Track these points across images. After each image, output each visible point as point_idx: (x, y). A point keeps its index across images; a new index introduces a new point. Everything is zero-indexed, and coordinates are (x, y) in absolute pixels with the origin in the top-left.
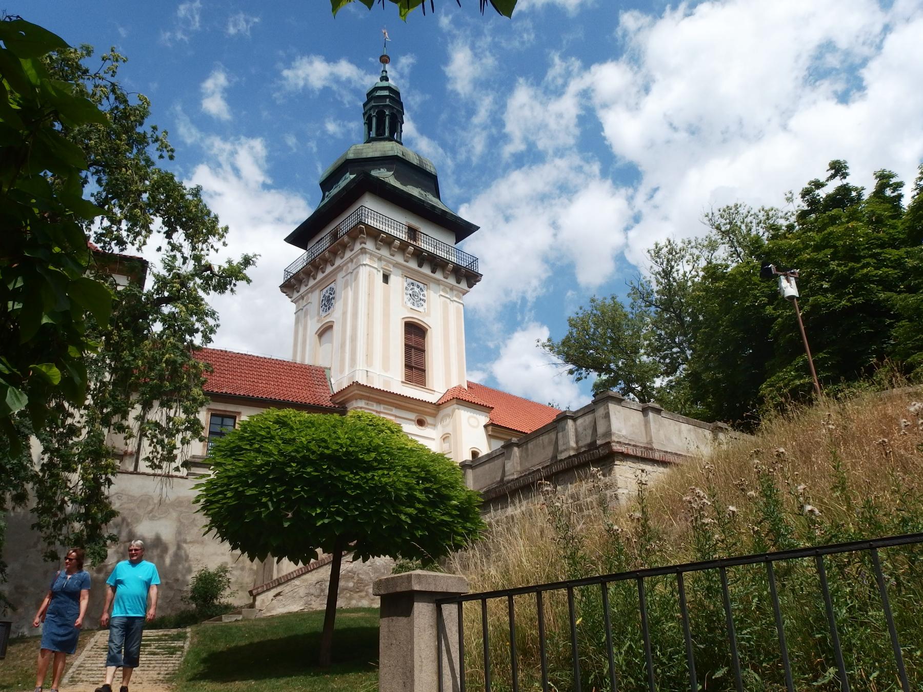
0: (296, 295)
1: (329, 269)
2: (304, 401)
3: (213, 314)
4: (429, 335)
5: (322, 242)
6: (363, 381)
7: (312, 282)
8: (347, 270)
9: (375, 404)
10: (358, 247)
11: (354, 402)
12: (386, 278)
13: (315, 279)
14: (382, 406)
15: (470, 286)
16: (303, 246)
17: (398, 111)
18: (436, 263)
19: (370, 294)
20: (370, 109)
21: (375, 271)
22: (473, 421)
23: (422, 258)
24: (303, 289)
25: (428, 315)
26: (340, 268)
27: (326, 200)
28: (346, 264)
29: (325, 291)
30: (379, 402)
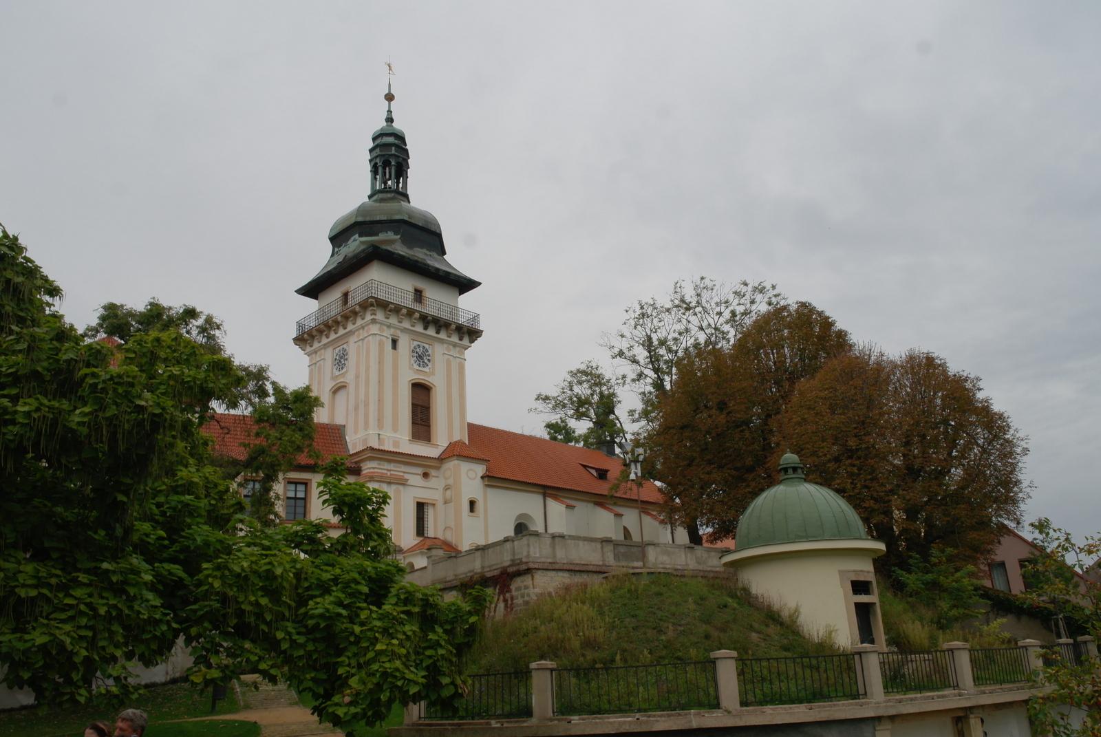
0: (309, 349)
1: (341, 332)
3: (191, 313)
5: (333, 296)
6: (376, 446)
7: (325, 341)
9: (386, 463)
10: (369, 317)
11: (368, 462)
14: (392, 465)
15: (472, 341)
18: (440, 324)
19: (381, 362)
20: (376, 157)
21: (384, 339)
22: (472, 474)
23: (426, 321)
24: (316, 345)
25: (433, 374)
26: (351, 333)
27: (339, 258)
29: (337, 350)
30: (389, 461)
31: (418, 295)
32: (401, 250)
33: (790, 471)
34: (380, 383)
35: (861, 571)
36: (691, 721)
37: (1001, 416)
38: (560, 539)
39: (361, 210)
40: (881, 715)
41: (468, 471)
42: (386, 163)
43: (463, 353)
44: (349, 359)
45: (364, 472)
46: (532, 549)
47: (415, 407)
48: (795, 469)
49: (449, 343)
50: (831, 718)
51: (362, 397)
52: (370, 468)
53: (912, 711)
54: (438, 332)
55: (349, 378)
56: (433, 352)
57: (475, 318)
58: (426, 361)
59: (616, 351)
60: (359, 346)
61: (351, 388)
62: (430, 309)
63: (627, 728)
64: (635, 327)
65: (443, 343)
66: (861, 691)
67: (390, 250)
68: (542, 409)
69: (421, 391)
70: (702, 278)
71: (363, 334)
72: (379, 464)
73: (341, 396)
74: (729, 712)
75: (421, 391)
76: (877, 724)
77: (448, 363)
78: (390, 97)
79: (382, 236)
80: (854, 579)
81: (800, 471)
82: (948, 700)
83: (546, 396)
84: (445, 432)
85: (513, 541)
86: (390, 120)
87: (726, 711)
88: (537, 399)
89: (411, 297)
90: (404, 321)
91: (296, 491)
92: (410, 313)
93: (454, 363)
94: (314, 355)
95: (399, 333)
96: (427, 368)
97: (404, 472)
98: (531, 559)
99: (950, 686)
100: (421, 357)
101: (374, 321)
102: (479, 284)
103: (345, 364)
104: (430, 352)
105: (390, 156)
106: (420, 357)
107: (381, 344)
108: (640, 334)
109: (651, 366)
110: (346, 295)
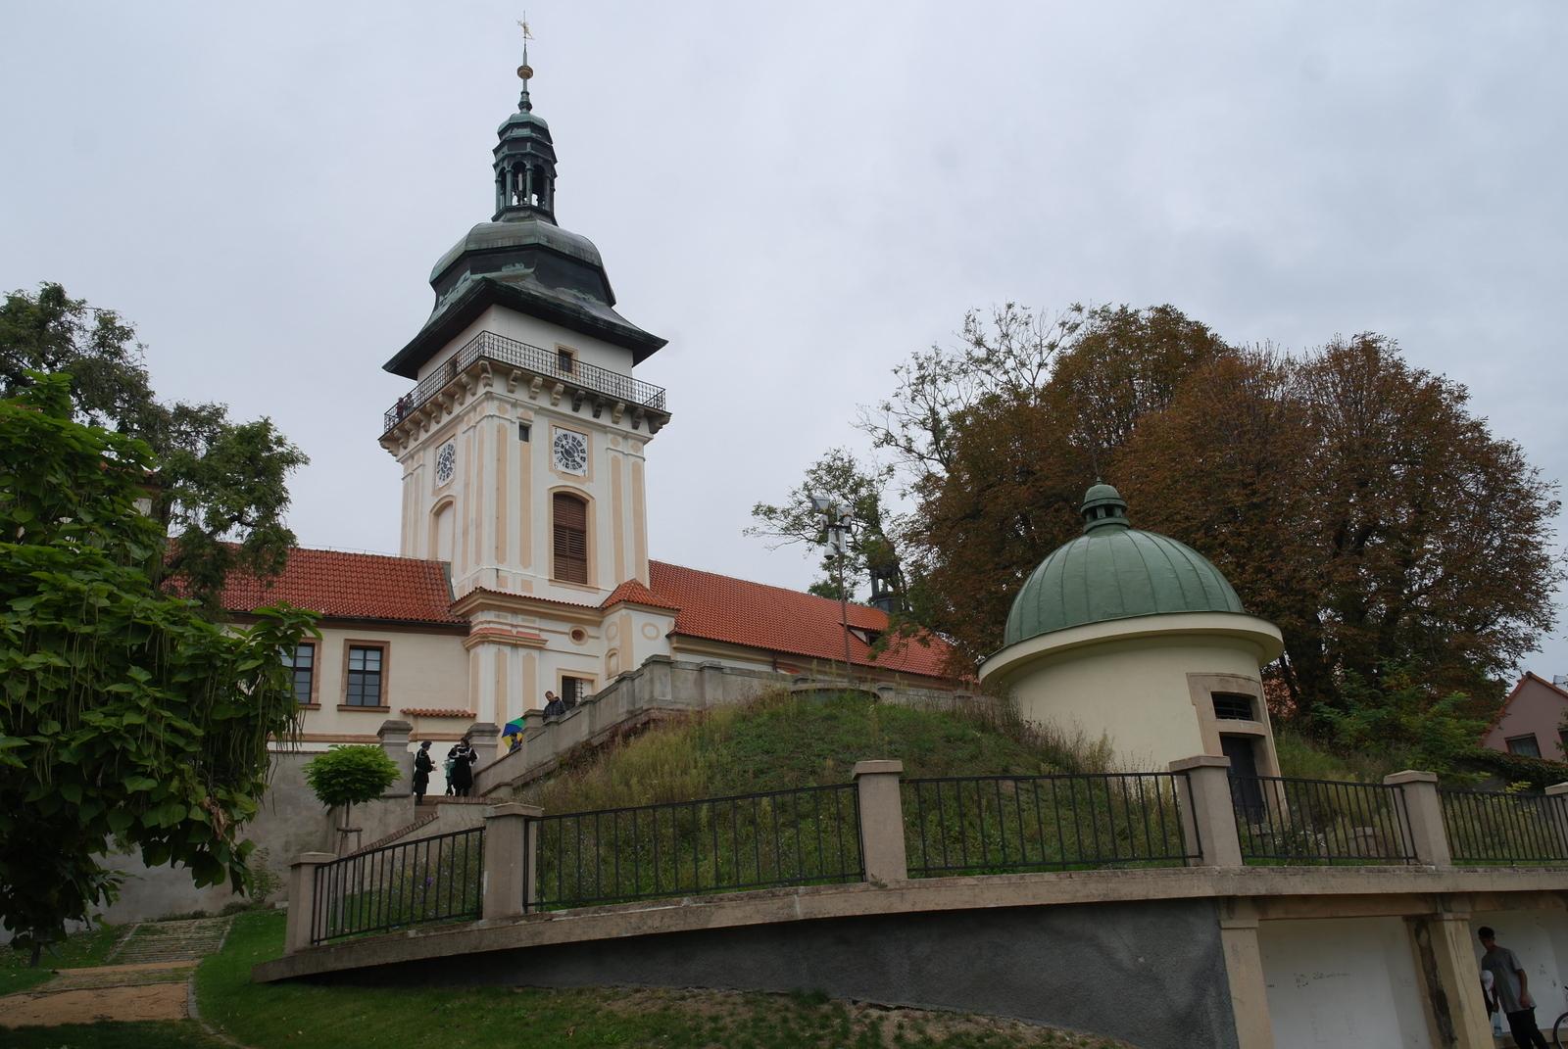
0: (402, 452)
1: (445, 419)
2: (409, 617)
4: (590, 507)
5: (436, 372)
7: (423, 436)
8: (469, 420)
9: (509, 616)
10: (481, 390)
12: (525, 431)
13: (427, 431)
14: (520, 617)
15: (654, 431)
16: (412, 374)
17: (546, 161)
18: (600, 403)
19: (500, 460)
20: (503, 160)
21: (507, 424)
22: (650, 631)
23: (579, 397)
24: (412, 445)
25: (590, 479)
26: (459, 419)
27: (443, 310)
28: (480, 403)
30: (515, 612)
31: (565, 358)
32: (534, 287)
33: (1101, 513)
34: (500, 490)
35: (1233, 676)
36: (791, 906)
37: (1506, 449)
38: (712, 671)
39: (476, 234)
40: (1231, 893)
41: (645, 625)
42: (519, 168)
43: (640, 449)
44: (457, 461)
45: (475, 629)
46: (658, 688)
47: (559, 530)
48: (1110, 510)
49: (617, 433)
50: (1113, 897)
51: (472, 514)
52: (482, 623)
53: (1303, 892)
54: (596, 416)
55: (456, 490)
56: (590, 445)
57: (659, 397)
58: (578, 459)
59: (881, 434)
60: (469, 436)
61: (459, 505)
62: (584, 379)
63: (657, 924)
64: (913, 400)
65: (606, 433)
66: (1191, 848)
67: (527, 297)
68: (765, 529)
69: (570, 509)
70: (1010, 306)
71: (474, 418)
72: (498, 616)
73: (447, 517)
74: (883, 887)
75: (570, 509)
76: (1224, 914)
77: (616, 463)
78: (525, 73)
79: (506, 271)
80: (1217, 689)
81: (1118, 512)
82: (1399, 881)
83: (769, 508)
84: (606, 573)
85: (633, 680)
86: (526, 105)
87: (875, 884)
88: (756, 512)
89: (553, 359)
90: (560, 405)
91: (365, 661)
92: (549, 384)
93: (626, 466)
94: (410, 462)
95: (531, 415)
96: (581, 470)
97: (541, 630)
98: (655, 705)
99: (1399, 858)
100: (570, 454)
101: (489, 396)
102: (665, 342)
103: (451, 469)
104: (585, 446)
105: (526, 158)
106: (568, 454)
107: (501, 431)
108: (921, 411)
109: (937, 457)
110: (454, 363)
